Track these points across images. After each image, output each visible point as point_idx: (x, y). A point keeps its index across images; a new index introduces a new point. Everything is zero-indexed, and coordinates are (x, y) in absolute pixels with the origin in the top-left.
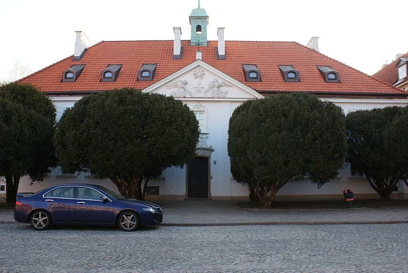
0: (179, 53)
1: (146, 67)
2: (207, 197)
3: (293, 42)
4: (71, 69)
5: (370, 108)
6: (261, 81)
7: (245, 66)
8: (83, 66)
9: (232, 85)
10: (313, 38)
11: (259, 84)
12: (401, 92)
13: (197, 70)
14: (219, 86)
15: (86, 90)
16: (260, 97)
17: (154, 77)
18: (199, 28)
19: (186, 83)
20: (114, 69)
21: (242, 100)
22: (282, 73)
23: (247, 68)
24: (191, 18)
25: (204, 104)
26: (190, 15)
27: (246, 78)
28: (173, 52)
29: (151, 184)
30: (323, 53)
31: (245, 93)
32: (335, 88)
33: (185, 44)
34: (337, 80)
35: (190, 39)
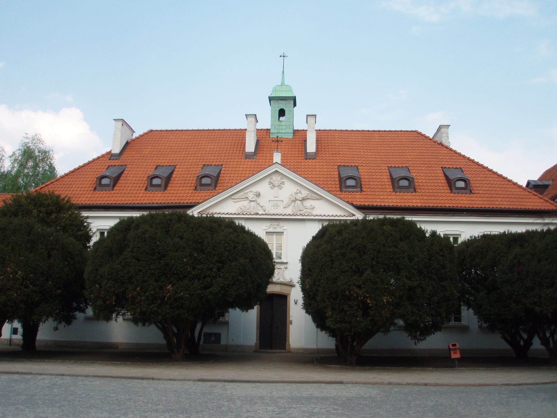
0: (252, 150)
1: (207, 171)
2: (285, 348)
3: (414, 131)
4: (157, 173)
5: (521, 229)
6: (362, 191)
7: (394, 169)
8: (173, 168)
14: (303, 200)
15: (123, 202)
16: (359, 216)
17: (212, 182)
18: (282, 113)
19: (259, 194)
20: (164, 173)
21: (328, 218)
22: (392, 179)
23: (344, 174)
24: (271, 99)
25: (282, 224)
26: (269, 95)
28: (244, 148)
29: (208, 329)
30: (454, 149)
31: (333, 209)
33: (263, 136)
34: (468, 188)
35: (269, 128)
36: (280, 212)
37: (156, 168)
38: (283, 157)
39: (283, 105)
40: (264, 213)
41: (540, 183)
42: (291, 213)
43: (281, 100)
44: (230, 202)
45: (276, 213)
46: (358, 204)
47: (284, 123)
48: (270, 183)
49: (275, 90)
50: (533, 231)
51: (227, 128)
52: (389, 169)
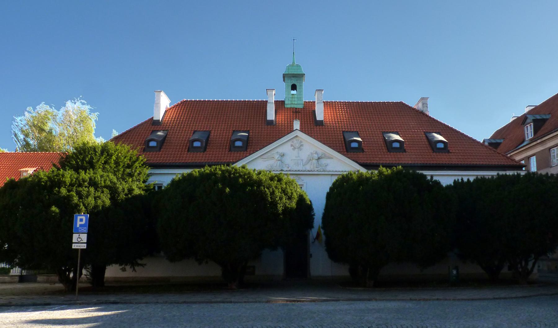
1: (196, 136)
9: (330, 158)
10: (423, 99)
11: (361, 155)
12: (515, 163)
13: (295, 140)
14: (319, 158)
17: (249, 147)
24: (284, 76)
25: (303, 177)
26: (284, 73)
27: (346, 149)
31: (344, 165)
32: (443, 159)
36: (301, 169)
37: (194, 133)
38: (301, 125)
39: (294, 80)
40: (288, 169)
41: (493, 141)
42: (309, 169)
43: (293, 77)
44: (260, 161)
45: (297, 169)
46: (362, 162)
47: (296, 96)
48: (292, 145)
49: (288, 68)
50: (502, 175)
51: (474, 138)
52: (425, 134)
